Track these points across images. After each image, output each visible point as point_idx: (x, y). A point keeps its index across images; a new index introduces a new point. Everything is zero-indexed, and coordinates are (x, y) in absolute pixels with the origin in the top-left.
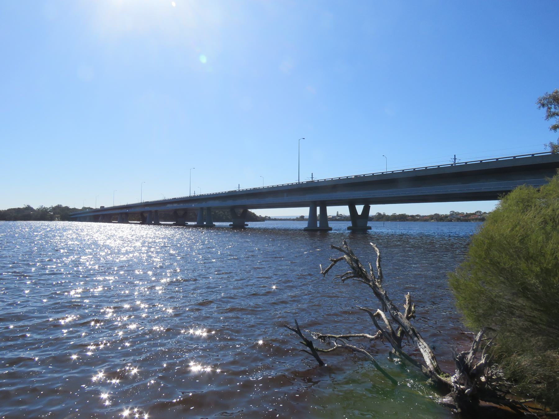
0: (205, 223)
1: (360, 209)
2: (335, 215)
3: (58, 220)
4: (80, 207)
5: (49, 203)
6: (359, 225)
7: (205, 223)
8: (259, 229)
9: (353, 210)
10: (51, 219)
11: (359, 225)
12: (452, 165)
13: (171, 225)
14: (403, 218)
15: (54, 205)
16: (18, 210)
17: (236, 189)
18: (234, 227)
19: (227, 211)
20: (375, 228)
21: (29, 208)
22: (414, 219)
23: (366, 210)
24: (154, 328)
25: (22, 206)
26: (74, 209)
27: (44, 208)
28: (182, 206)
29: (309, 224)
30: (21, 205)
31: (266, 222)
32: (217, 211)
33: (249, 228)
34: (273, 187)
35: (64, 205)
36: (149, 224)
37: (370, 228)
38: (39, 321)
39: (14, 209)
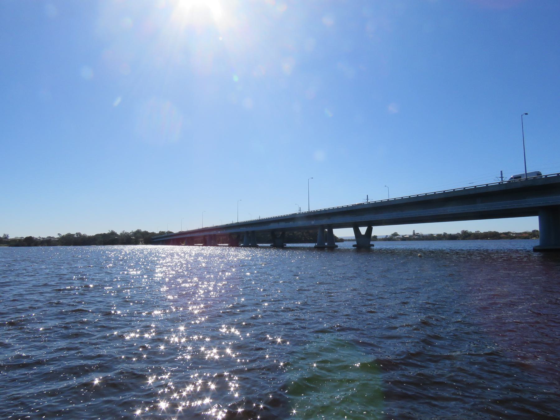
0: (326, 244)
1: (363, 230)
2: (412, 234)
3: (142, 244)
4: (157, 232)
5: (130, 229)
6: (364, 244)
7: (326, 244)
8: (302, 247)
9: (357, 232)
10: (136, 243)
11: (364, 244)
12: (499, 183)
13: (310, 249)
14: (494, 236)
15: (135, 230)
16: (104, 235)
17: (297, 212)
18: (320, 248)
19: (304, 232)
20: (377, 246)
21: (113, 234)
22: (507, 236)
23: (369, 231)
24: (239, 333)
25: (107, 232)
26: (153, 234)
27: (126, 233)
28: (250, 229)
29: (540, 241)
30: (106, 230)
31: (345, 242)
32: (295, 232)
33: (339, 250)
34: (321, 211)
35: (143, 230)
36: (440, 250)
37: (373, 245)
38: (113, 398)
39: (101, 235)
